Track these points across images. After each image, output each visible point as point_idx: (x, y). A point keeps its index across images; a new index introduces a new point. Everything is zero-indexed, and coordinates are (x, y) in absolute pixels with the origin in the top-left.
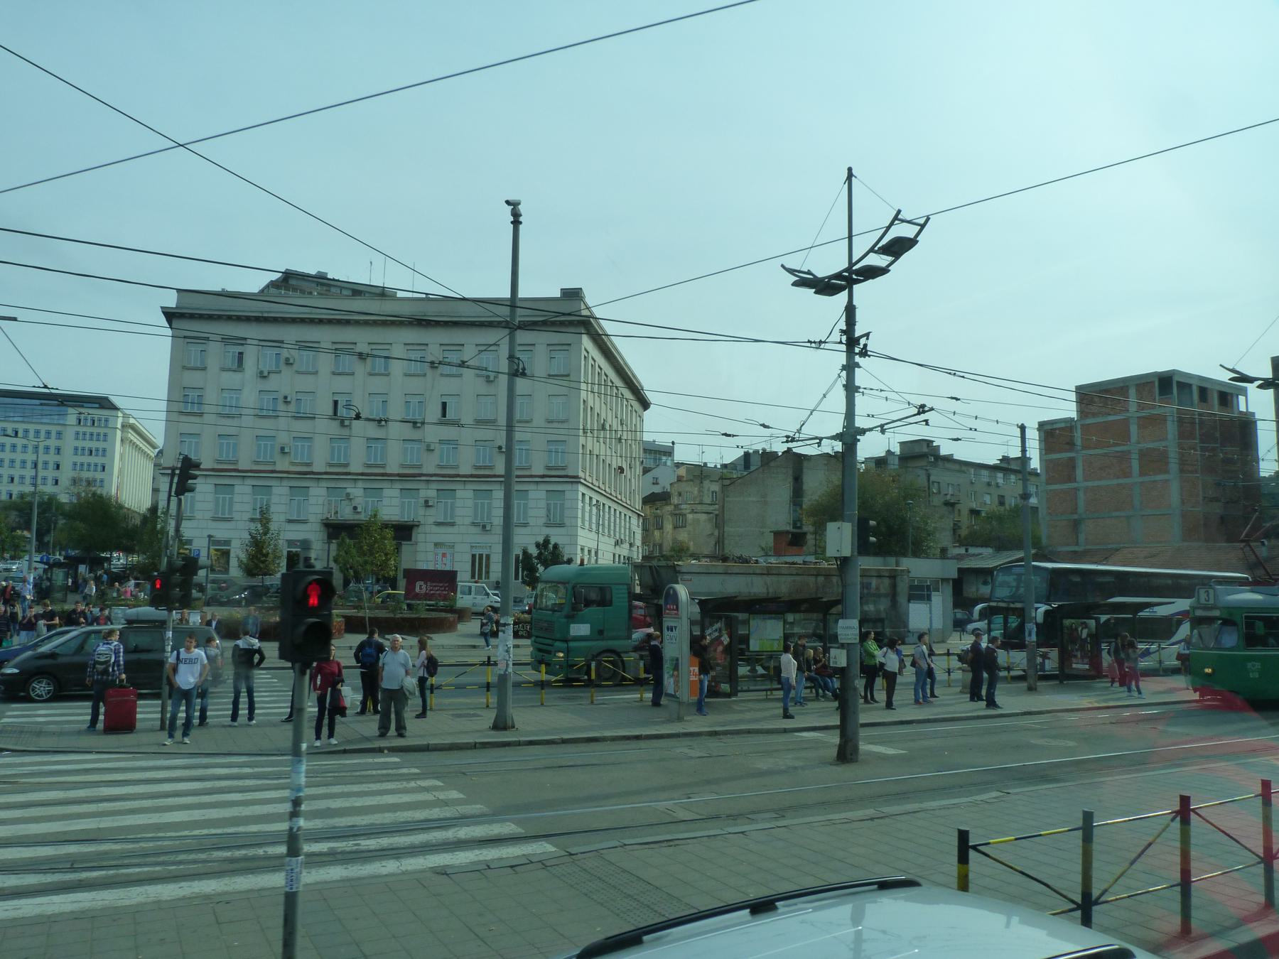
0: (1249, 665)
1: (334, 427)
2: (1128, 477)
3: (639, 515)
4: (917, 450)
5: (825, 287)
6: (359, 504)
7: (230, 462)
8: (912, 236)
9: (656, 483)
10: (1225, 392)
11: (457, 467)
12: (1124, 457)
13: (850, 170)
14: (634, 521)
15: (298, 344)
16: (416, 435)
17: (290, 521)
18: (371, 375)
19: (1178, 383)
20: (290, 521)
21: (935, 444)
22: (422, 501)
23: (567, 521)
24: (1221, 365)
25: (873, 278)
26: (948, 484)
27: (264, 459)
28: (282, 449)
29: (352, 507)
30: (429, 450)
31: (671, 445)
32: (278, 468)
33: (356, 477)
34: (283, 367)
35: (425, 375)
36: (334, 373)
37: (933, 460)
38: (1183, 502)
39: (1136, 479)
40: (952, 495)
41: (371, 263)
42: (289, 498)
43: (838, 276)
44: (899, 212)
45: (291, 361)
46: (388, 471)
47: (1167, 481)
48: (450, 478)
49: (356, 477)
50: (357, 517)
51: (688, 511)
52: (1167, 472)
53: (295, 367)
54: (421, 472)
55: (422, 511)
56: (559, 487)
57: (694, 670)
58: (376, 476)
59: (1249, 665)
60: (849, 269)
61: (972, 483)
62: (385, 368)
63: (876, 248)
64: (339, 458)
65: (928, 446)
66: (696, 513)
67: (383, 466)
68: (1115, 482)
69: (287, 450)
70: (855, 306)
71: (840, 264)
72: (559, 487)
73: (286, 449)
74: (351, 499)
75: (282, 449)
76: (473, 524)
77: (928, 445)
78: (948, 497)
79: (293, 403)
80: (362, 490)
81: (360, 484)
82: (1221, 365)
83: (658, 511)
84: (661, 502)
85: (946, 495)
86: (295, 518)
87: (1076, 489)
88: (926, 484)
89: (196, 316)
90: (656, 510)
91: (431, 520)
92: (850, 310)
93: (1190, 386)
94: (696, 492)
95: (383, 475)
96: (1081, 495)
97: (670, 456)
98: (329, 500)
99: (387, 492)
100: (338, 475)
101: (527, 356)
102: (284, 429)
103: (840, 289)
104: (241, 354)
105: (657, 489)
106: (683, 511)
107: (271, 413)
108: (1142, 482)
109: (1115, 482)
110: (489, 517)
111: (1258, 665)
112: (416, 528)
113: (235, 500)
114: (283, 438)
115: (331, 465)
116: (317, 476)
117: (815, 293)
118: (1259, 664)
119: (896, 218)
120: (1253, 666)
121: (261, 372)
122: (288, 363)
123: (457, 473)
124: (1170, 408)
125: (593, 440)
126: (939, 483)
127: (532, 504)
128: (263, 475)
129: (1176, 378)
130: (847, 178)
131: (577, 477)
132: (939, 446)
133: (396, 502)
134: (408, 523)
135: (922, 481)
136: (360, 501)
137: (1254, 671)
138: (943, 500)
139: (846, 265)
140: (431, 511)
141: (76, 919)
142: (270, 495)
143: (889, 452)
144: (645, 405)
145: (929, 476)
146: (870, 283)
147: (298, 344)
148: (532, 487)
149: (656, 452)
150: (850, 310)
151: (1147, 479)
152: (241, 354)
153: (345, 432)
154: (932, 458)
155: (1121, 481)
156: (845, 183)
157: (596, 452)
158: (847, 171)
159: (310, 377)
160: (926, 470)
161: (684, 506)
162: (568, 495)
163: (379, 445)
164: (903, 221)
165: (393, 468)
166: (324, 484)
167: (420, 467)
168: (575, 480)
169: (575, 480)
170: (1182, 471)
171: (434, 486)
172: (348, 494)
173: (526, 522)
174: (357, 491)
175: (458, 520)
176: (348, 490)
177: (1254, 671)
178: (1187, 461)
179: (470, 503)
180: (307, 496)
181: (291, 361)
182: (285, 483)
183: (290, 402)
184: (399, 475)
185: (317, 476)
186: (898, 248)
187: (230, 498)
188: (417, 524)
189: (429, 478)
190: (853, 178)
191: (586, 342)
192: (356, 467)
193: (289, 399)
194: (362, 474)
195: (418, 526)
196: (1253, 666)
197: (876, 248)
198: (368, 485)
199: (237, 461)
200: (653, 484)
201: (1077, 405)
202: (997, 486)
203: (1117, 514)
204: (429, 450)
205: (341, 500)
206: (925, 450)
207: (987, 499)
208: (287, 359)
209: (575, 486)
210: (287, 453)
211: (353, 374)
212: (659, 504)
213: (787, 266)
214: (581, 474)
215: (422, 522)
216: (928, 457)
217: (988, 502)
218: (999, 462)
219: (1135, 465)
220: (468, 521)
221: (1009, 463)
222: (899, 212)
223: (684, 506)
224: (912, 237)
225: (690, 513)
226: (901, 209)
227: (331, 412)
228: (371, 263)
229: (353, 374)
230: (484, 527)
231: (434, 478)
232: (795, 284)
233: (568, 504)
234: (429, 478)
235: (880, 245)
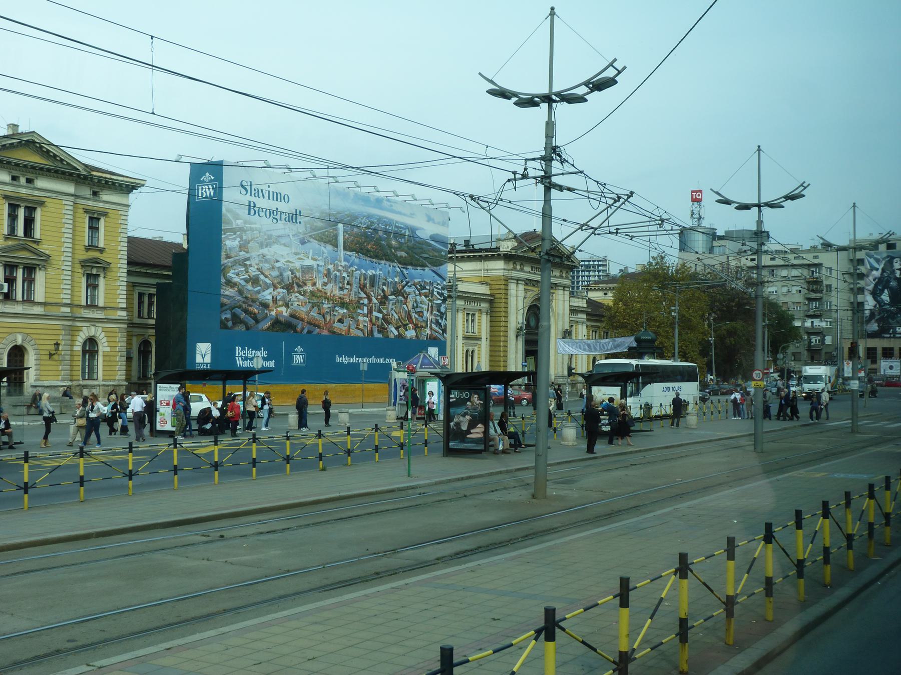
24: (480, 74)
71: (545, 90)
92: (550, 126)
150: (550, 126)
186: (599, 85)
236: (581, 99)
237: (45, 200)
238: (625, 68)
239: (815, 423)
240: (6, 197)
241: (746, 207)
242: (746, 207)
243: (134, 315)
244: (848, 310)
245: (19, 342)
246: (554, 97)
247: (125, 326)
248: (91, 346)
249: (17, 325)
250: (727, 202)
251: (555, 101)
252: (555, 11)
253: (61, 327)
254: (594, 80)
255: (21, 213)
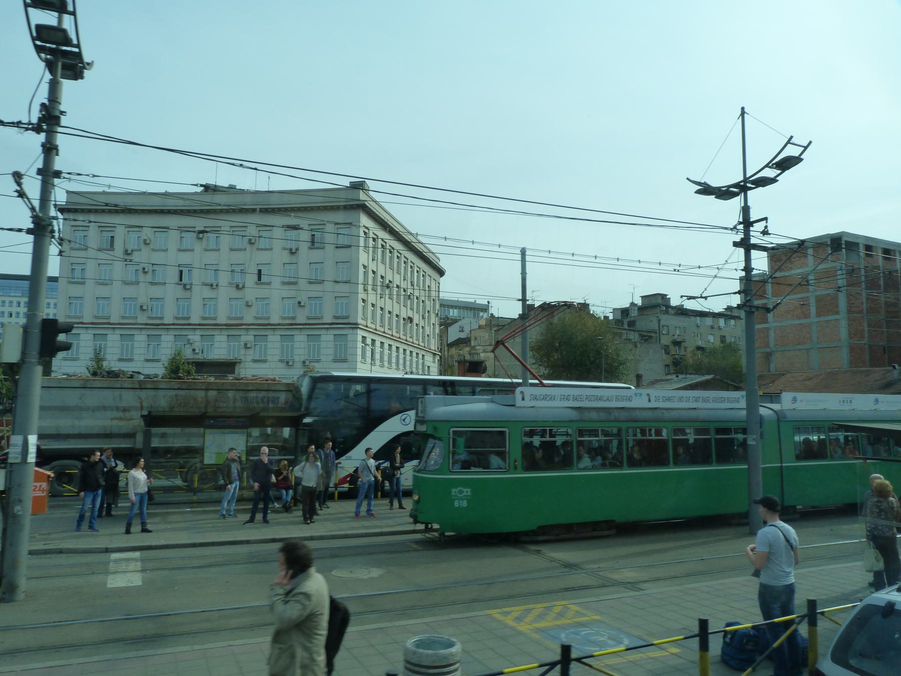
0: (454, 491)
1: (179, 292)
2: (807, 318)
3: (434, 354)
4: (654, 302)
5: (723, 194)
6: (197, 347)
7: (184, 318)
8: (797, 155)
9: (462, 331)
10: (889, 249)
11: (268, 318)
12: (804, 305)
13: (743, 109)
14: (429, 359)
15: (179, 229)
16: (239, 294)
17: (147, 360)
18: (206, 250)
19: (846, 242)
20: (147, 360)
21: (668, 297)
22: (242, 344)
23: (349, 358)
24: (688, 179)
25: (763, 186)
26: (676, 327)
27: (156, 315)
28: (141, 307)
29: (192, 349)
30: (248, 306)
31: (487, 304)
32: (140, 321)
33: (195, 327)
34: (142, 246)
35: (245, 250)
36: (180, 250)
37: (664, 309)
38: (850, 337)
39: (814, 319)
40: (678, 335)
41: (269, 177)
42: (147, 343)
43: (736, 185)
44: (792, 137)
45: (148, 242)
46: (218, 322)
47: (837, 320)
48: (265, 326)
49: (195, 327)
50: (196, 356)
51: (480, 351)
52: (837, 313)
53: (151, 246)
54: (242, 323)
55: (243, 351)
56: (263, 333)
57: (41, 486)
58: (209, 326)
59: (454, 491)
60: (746, 180)
61: (698, 326)
62: (216, 245)
63: (771, 165)
64: (183, 313)
65: (663, 298)
66: (487, 352)
67: (215, 319)
68: (797, 322)
69: (145, 308)
70: (749, 206)
72: (263, 333)
73: (144, 307)
74: (191, 344)
75: (141, 307)
76: (281, 361)
77: (662, 297)
78: (676, 337)
79: (150, 273)
80: (199, 336)
81: (198, 332)
82: (688, 179)
83: (461, 351)
84: (463, 345)
85: (674, 335)
86: (152, 358)
87: (768, 329)
88: (657, 328)
89: (79, 210)
90: (460, 350)
91: (249, 358)
92: (746, 210)
93: (857, 244)
94: (487, 337)
95: (215, 325)
96: (772, 333)
97: (486, 312)
98: (176, 344)
99: (217, 338)
100: (182, 325)
101: (294, 234)
102: (143, 293)
103: (735, 195)
104: (112, 237)
105: (463, 335)
106: (478, 351)
107: (80, 280)
108: (818, 322)
109: (797, 322)
110: (292, 356)
111: (467, 491)
112: (238, 364)
113: (81, 345)
114: (142, 300)
115: (177, 318)
116: (166, 327)
117: (715, 197)
118: (469, 490)
119: (789, 142)
120: (461, 492)
121: (126, 251)
122: (146, 243)
123: (269, 323)
124: (839, 263)
125: (376, 296)
126: (668, 326)
127: (323, 345)
128: (126, 327)
129: (844, 239)
130: (741, 115)
131: (357, 324)
132: (670, 298)
133: (224, 345)
134: (232, 361)
135: (654, 325)
136: (197, 345)
137: (461, 498)
138: (671, 339)
139: (742, 178)
140: (251, 352)
141: (22, 670)
142: (214, 342)
143: (632, 304)
144: (441, 273)
145: (659, 321)
146: (760, 189)
147: (179, 229)
148: (324, 332)
149: (475, 309)
151: (822, 319)
152: (112, 237)
153: (187, 294)
154: (664, 308)
155: (802, 321)
156: (738, 119)
157: (387, 309)
158: (740, 110)
159: (188, 253)
160: (657, 316)
161: (478, 348)
162: (350, 338)
163: (212, 302)
164: (803, 147)
165: (222, 320)
166: (173, 333)
167: (242, 318)
168: (355, 326)
169: (355, 326)
170: (849, 311)
171: (252, 333)
172: (189, 340)
173: (265, 359)
174: (195, 337)
175: (269, 358)
176: (189, 337)
177: (461, 498)
178: (853, 304)
179: (331, 345)
180: (133, 341)
181: (148, 242)
182: (144, 332)
183: (147, 272)
184: (226, 325)
185: (166, 327)
186: (785, 164)
187: (265, 345)
188: (239, 361)
189: (248, 327)
190: (746, 114)
191: (365, 220)
192: (195, 320)
193: (146, 270)
194: (199, 325)
195: (240, 363)
196: (461, 492)
197: (771, 165)
198: (177, 333)
199: (110, 316)
200: (460, 331)
201: (768, 259)
202: (720, 328)
203: (798, 347)
204: (248, 306)
205: (185, 344)
206: (660, 301)
207: (711, 338)
208: (145, 241)
209: (355, 331)
210: (145, 310)
211: (193, 250)
212: (461, 345)
213: (691, 179)
214: (360, 321)
215: (243, 360)
216: (661, 307)
217: (712, 340)
218: (724, 310)
219: (813, 310)
220: (277, 358)
221: (731, 311)
222: (792, 137)
223: (478, 348)
224: (797, 155)
225: (482, 352)
226: (812, 141)
227: (177, 279)
228: (269, 177)
229: (193, 250)
230: (287, 363)
231: (251, 327)
232: (698, 192)
233: (350, 345)
234: (248, 327)
235: (774, 162)
236: (773, 181)
238: (810, 143)
246: (749, 185)
251: (751, 189)
252: (746, 110)
254: (774, 162)
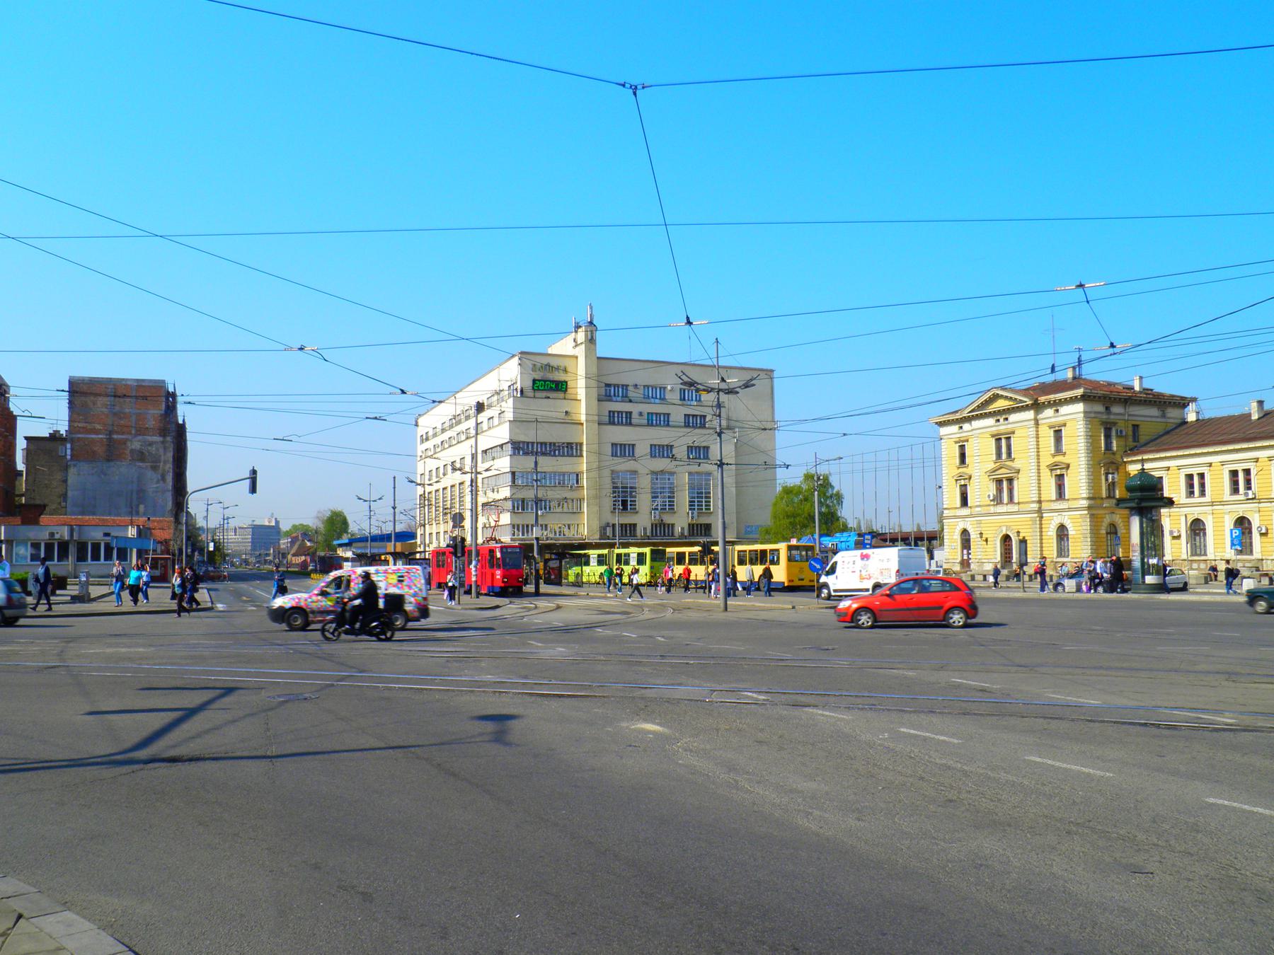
92: (536, 463)
237: (1118, 421)
239: (520, 513)
240: (993, 436)
241: (365, 501)
242: (365, 501)
243: (1182, 495)
244: (727, 464)
245: (1004, 532)
247: (1086, 512)
248: (1062, 532)
249: (1004, 520)
250: (361, 499)
253: (1029, 519)
255: (1004, 442)
